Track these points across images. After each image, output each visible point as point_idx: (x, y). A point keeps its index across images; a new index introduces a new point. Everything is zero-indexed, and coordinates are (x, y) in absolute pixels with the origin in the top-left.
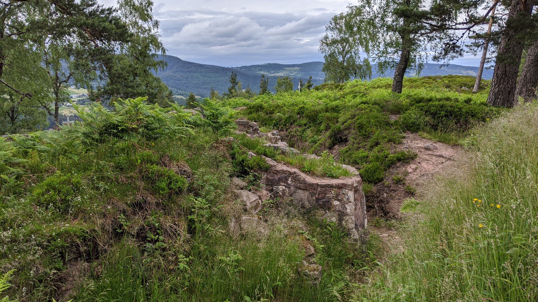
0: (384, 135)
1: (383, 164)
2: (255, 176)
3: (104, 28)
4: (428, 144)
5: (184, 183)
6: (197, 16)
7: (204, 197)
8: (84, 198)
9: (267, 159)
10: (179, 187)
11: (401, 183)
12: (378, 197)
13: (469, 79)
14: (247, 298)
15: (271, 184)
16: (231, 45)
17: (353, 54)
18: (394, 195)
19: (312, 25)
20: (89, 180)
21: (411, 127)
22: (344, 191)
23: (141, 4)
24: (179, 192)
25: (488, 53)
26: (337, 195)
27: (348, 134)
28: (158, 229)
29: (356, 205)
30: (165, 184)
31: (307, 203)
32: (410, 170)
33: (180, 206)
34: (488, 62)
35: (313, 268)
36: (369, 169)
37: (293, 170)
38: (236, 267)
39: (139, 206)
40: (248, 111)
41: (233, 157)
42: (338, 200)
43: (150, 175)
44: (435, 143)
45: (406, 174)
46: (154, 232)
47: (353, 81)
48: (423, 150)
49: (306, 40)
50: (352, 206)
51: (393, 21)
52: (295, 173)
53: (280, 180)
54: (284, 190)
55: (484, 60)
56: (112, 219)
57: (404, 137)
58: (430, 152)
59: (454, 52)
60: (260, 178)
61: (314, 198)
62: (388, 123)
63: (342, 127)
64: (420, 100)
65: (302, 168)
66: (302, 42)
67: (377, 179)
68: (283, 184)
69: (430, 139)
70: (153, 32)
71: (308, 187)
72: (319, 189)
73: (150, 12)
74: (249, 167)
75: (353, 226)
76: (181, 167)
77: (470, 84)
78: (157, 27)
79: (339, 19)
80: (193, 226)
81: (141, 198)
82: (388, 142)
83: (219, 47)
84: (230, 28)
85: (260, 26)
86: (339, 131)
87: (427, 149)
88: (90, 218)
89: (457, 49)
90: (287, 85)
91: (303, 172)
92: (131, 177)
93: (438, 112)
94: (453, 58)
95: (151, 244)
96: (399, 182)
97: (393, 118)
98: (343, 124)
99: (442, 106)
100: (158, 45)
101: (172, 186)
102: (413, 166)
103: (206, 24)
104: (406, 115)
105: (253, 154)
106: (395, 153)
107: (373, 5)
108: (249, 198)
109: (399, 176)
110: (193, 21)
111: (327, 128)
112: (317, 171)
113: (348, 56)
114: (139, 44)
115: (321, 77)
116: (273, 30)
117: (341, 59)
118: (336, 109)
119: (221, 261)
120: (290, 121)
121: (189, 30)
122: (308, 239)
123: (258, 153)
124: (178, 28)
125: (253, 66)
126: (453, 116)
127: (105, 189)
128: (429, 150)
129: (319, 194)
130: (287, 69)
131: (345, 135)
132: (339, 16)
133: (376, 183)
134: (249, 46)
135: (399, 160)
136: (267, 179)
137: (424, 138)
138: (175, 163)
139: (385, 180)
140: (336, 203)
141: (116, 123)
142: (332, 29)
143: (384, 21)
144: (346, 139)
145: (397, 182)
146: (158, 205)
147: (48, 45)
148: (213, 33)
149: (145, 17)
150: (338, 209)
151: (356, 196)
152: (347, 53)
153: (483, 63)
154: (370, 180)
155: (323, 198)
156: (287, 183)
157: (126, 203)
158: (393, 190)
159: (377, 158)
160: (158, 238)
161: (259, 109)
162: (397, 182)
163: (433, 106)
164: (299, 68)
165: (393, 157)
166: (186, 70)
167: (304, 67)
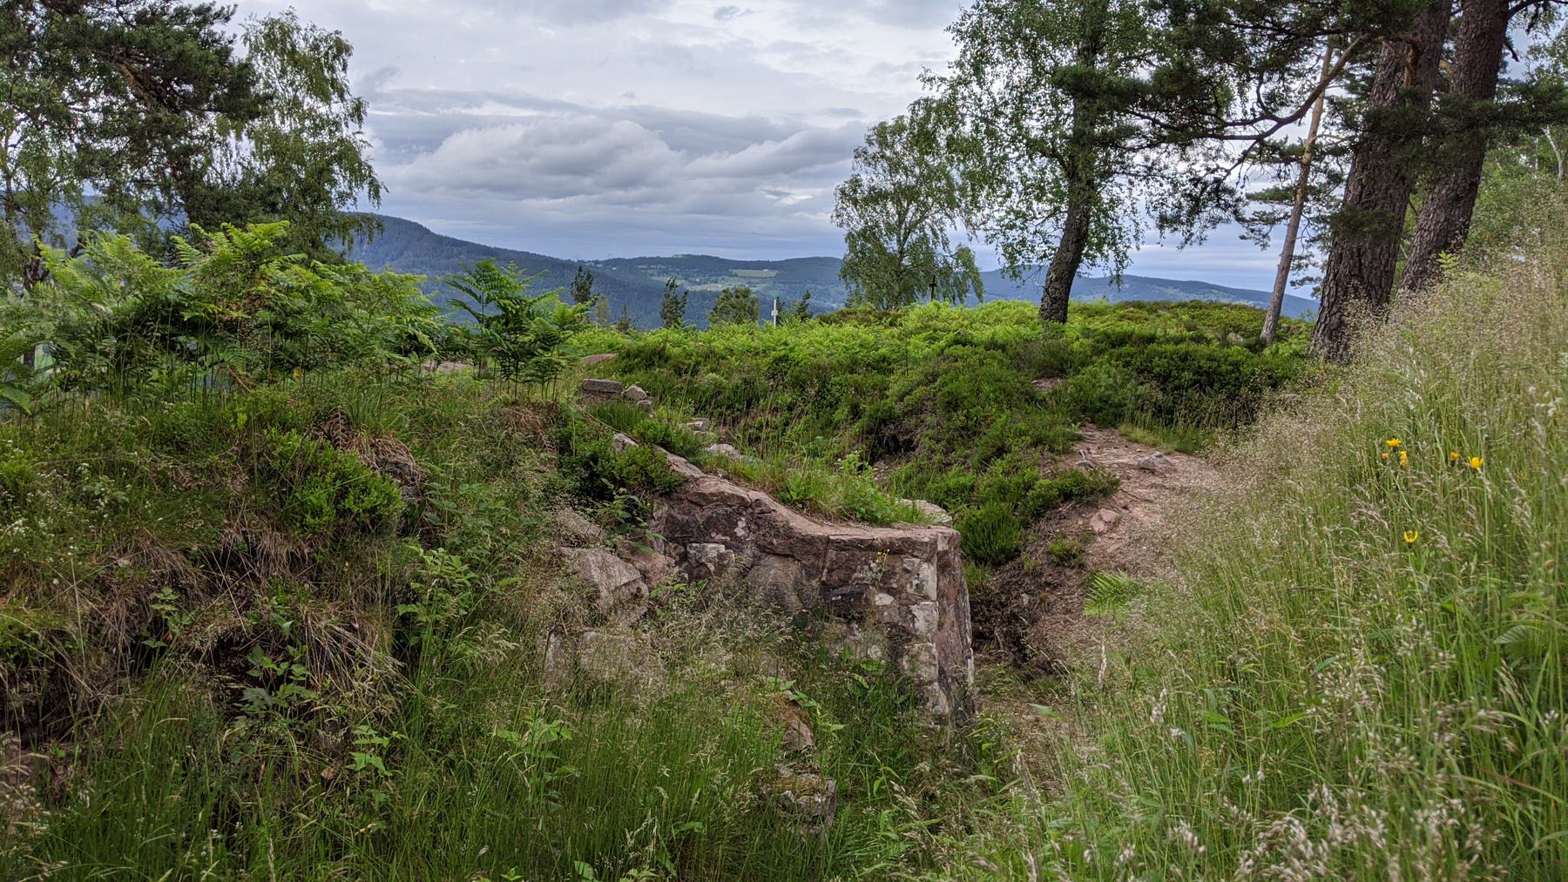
0: (1022, 426)
1: (1021, 508)
2: (631, 507)
3: (181, 54)
4: (1151, 456)
5: (390, 499)
6: (489, 110)
7: (454, 550)
8: (35, 527)
9: (671, 458)
10: (373, 510)
11: (1073, 562)
12: (1003, 605)
13: (1245, 315)
14: (587, 871)
15: (681, 536)
16: (582, 197)
17: (928, 231)
18: (1052, 598)
19: (813, 155)
20: (61, 471)
21: (1099, 410)
22: (909, 562)
23: (315, 48)
24: (373, 525)
25: (1298, 242)
26: (888, 575)
27: (916, 427)
28: (291, 643)
29: (943, 612)
30: (324, 497)
31: (794, 598)
32: (1099, 526)
33: (374, 570)
34: (1299, 267)
35: (808, 788)
36: (978, 521)
37: (753, 495)
38: (551, 766)
39: (229, 566)
40: (623, 364)
41: (564, 446)
42: (890, 591)
43: (275, 464)
44: (1168, 454)
45: (1088, 536)
46: (277, 652)
47: (922, 307)
48: (1133, 473)
49: (800, 195)
50: (931, 611)
51: (1045, 129)
52: (758, 502)
53: (710, 524)
54: (721, 556)
55: (1288, 261)
56: (132, 602)
57: (1080, 439)
58: (1158, 481)
59: (1218, 206)
60: (647, 516)
61: (814, 583)
62: (1032, 398)
63: (898, 409)
64: (1123, 340)
65: (780, 492)
66: (787, 201)
67: (1002, 550)
68: (720, 537)
69: (1154, 445)
70: (346, 132)
71: (797, 548)
72: (832, 554)
73: (340, 75)
74: (613, 479)
75: (934, 672)
76: (384, 453)
77: (1250, 327)
78: (360, 119)
79: (893, 133)
80: (413, 642)
81: (241, 539)
82: (1035, 444)
83: (545, 202)
84: (586, 148)
85: (672, 148)
86: (887, 419)
87: (1146, 469)
88: (48, 594)
89: (1226, 197)
90: (741, 307)
91: (784, 502)
92: (211, 470)
93: (1174, 373)
94: (1215, 222)
95: (262, 692)
96: (1066, 559)
97: (1045, 387)
98: (901, 399)
99: (1185, 358)
100: (359, 172)
101: (349, 503)
102: (1109, 515)
103: (516, 134)
104: (1084, 376)
105: (627, 440)
106: (1054, 476)
107: (990, 78)
108: (608, 571)
109: (1068, 542)
110: (476, 124)
111: (856, 413)
112: (826, 501)
113: (914, 237)
114: (302, 163)
115: (836, 296)
116: (708, 162)
117: (892, 246)
118: (882, 365)
119: (504, 745)
120: (748, 398)
121: (462, 147)
122: (794, 703)
123: (642, 438)
124: (429, 139)
125: (642, 260)
126: (1216, 386)
127: (114, 506)
128: (1153, 472)
129: (830, 571)
130: (740, 272)
131: (907, 432)
132: (891, 123)
133: (999, 564)
134: (633, 203)
135: (1067, 496)
136: (670, 520)
137: (1136, 441)
138: (364, 440)
139: (1024, 556)
140: (882, 599)
141: (172, 297)
142: (872, 160)
143: (1020, 128)
144: (911, 441)
145: (1062, 559)
146: (295, 562)
147: (17, 151)
148: (533, 161)
149: (324, 87)
150: (887, 619)
151: (945, 581)
152: (909, 231)
153: (1285, 269)
154: (979, 553)
155: (844, 583)
156: (733, 536)
157: (186, 552)
158: (1048, 584)
159: (1003, 490)
160: (290, 672)
161: (656, 359)
162: (1062, 559)
163: (1161, 355)
164: (773, 274)
165: (1050, 487)
166: (443, 261)
167: (786, 269)
